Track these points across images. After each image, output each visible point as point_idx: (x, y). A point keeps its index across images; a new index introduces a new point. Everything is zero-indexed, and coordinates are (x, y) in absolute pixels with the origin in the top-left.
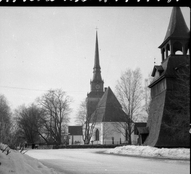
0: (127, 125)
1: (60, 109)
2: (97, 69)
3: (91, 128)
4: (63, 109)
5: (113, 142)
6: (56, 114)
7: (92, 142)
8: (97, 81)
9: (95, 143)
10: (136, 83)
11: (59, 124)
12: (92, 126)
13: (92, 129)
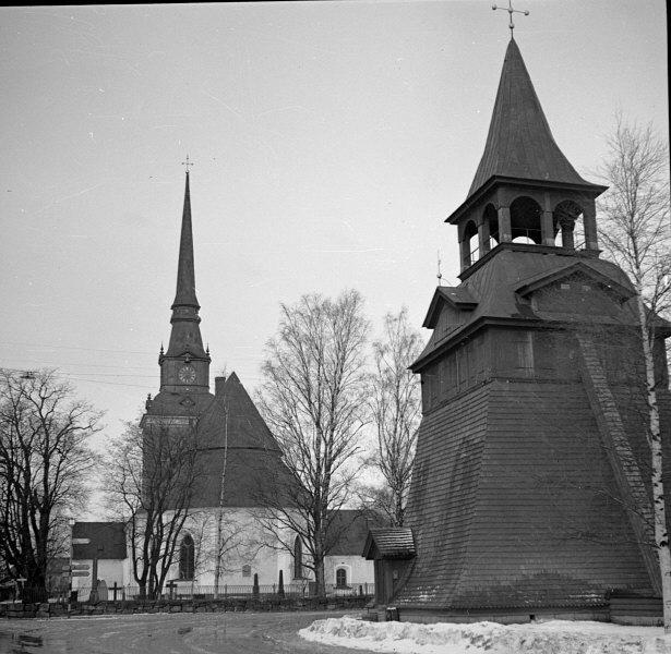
0: (311, 518)
1: (47, 457)
2: (185, 310)
3: (171, 533)
4: (56, 457)
5: (256, 587)
6: (28, 476)
7: (171, 585)
8: (186, 352)
9: (184, 588)
10: (343, 359)
11: (38, 516)
12: (173, 522)
13: (173, 534)
